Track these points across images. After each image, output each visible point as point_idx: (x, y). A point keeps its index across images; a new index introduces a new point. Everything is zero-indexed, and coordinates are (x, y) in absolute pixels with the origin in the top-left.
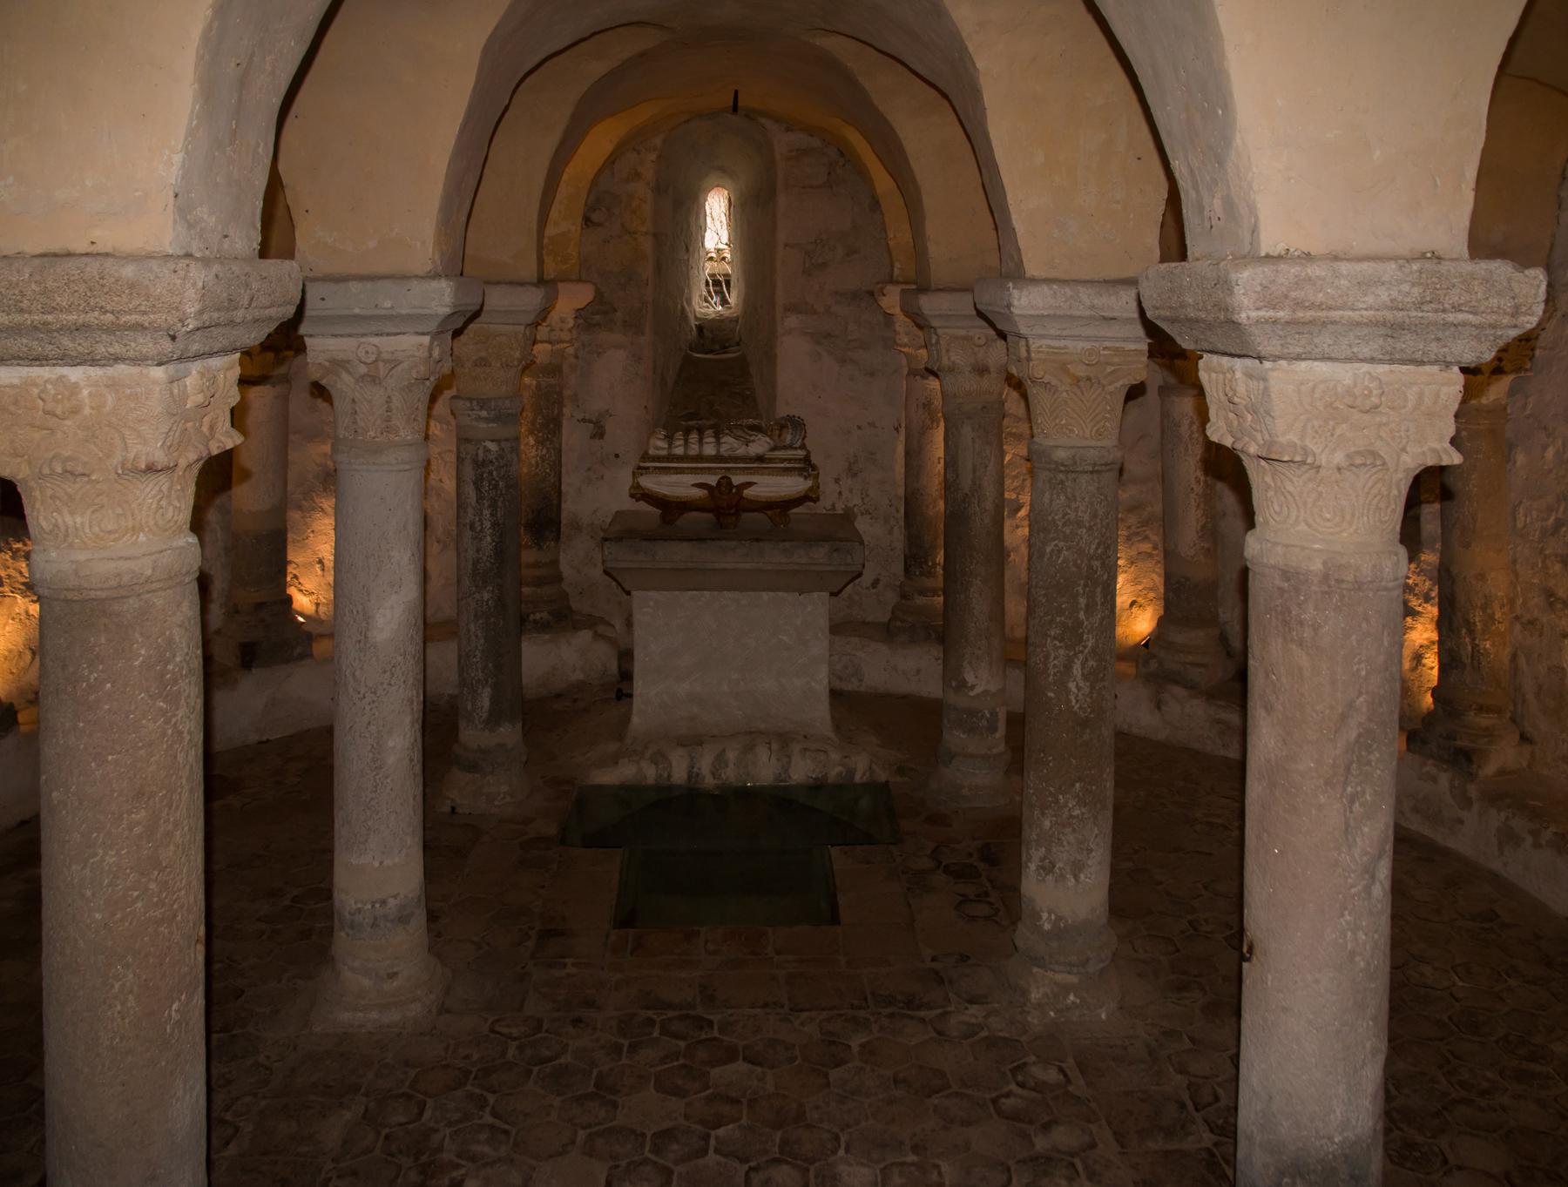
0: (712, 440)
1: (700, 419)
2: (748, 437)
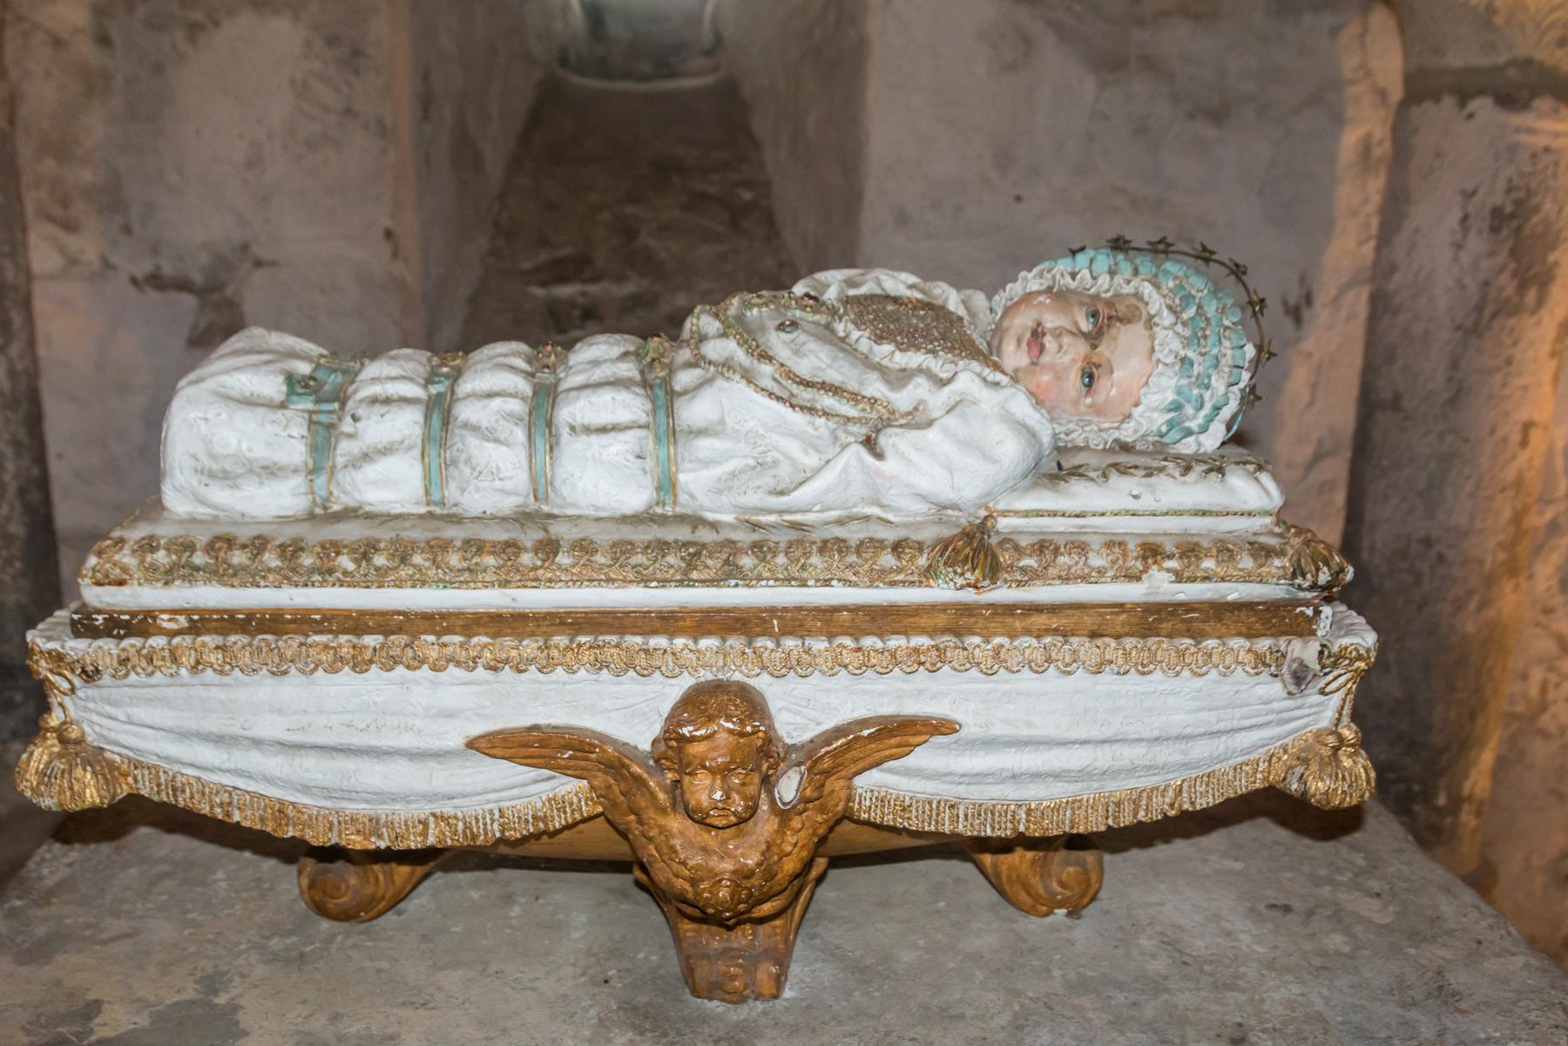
0: (629, 406)
1: (595, 279)
2: (875, 387)
